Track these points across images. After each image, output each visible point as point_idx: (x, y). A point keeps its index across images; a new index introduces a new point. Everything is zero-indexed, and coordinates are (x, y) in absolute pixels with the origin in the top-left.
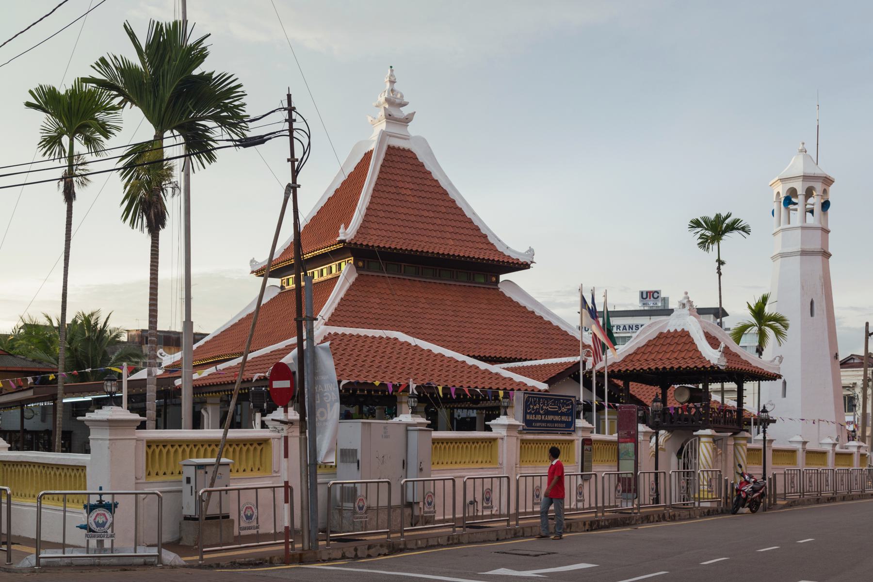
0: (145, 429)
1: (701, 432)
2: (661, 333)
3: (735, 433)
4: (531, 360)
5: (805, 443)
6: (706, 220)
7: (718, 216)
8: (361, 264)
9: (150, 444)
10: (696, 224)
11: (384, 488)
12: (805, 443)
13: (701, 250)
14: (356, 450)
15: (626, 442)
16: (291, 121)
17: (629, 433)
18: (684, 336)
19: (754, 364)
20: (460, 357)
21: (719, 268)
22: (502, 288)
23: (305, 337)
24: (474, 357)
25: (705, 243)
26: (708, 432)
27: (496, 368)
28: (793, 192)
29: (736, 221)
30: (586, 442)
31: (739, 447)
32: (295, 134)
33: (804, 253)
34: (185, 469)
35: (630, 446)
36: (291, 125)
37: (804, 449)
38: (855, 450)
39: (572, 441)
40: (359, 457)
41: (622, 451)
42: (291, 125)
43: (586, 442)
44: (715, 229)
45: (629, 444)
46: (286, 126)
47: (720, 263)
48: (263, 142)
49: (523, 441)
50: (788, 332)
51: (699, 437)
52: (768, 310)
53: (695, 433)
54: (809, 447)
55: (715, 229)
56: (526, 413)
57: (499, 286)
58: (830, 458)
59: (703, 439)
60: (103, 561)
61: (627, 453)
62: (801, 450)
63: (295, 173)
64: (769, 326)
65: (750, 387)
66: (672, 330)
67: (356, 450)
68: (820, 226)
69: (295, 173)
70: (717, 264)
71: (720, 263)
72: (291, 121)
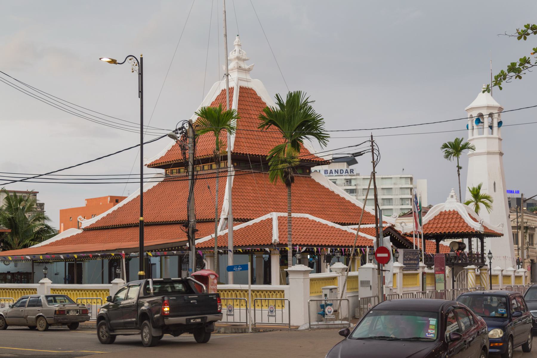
0: (320, 272)
1: (469, 267)
2: (441, 212)
3: (481, 267)
4: (365, 224)
5: (502, 271)
6: (449, 143)
7: (456, 140)
8: (235, 164)
9: (312, 280)
10: (445, 146)
11: (376, 298)
12: (502, 271)
13: (446, 160)
14: (369, 281)
15: (439, 274)
16: (372, 146)
17: (441, 269)
18: (455, 214)
19: (489, 228)
20: (331, 224)
21: (458, 171)
22: (313, 176)
23: (360, 233)
24: (339, 224)
25: (448, 155)
26: (473, 266)
27: (344, 228)
28: (481, 115)
29: (467, 144)
30: (424, 274)
31: (483, 275)
32: (374, 151)
33: (489, 153)
34: (323, 291)
35: (442, 275)
36: (372, 147)
37: (502, 274)
38: (522, 274)
39: (418, 274)
40: (371, 284)
41: (437, 278)
42: (372, 147)
43: (424, 274)
44: (456, 148)
45: (441, 275)
46: (371, 148)
47: (459, 168)
48: (362, 155)
49: (404, 275)
50: (493, 205)
51: (468, 269)
52: (482, 193)
53: (465, 268)
54: (504, 273)
55: (456, 148)
56: (404, 260)
57: (311, 175)
58: (513, 278)
59: (470, 271)
60: (330, 326)
61: (440, 279)
62: (500, 275)
63: (374, 168)
64: (482, 202)
65: (487, 240)
66: (447, 210)
67: (369, 281)
68: (497, 137)
69: (374, 168)
70: (457, 168)
71: (459, 168)
72: (372, 146)
